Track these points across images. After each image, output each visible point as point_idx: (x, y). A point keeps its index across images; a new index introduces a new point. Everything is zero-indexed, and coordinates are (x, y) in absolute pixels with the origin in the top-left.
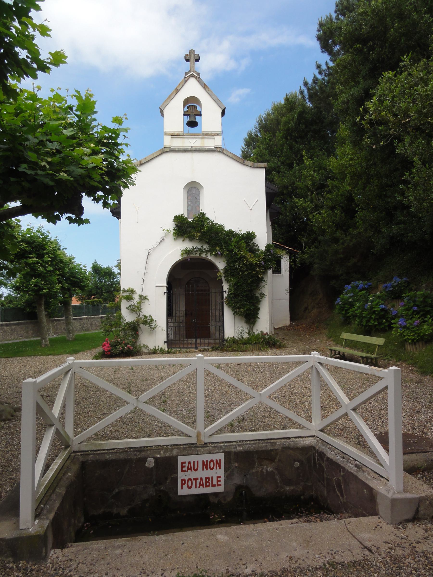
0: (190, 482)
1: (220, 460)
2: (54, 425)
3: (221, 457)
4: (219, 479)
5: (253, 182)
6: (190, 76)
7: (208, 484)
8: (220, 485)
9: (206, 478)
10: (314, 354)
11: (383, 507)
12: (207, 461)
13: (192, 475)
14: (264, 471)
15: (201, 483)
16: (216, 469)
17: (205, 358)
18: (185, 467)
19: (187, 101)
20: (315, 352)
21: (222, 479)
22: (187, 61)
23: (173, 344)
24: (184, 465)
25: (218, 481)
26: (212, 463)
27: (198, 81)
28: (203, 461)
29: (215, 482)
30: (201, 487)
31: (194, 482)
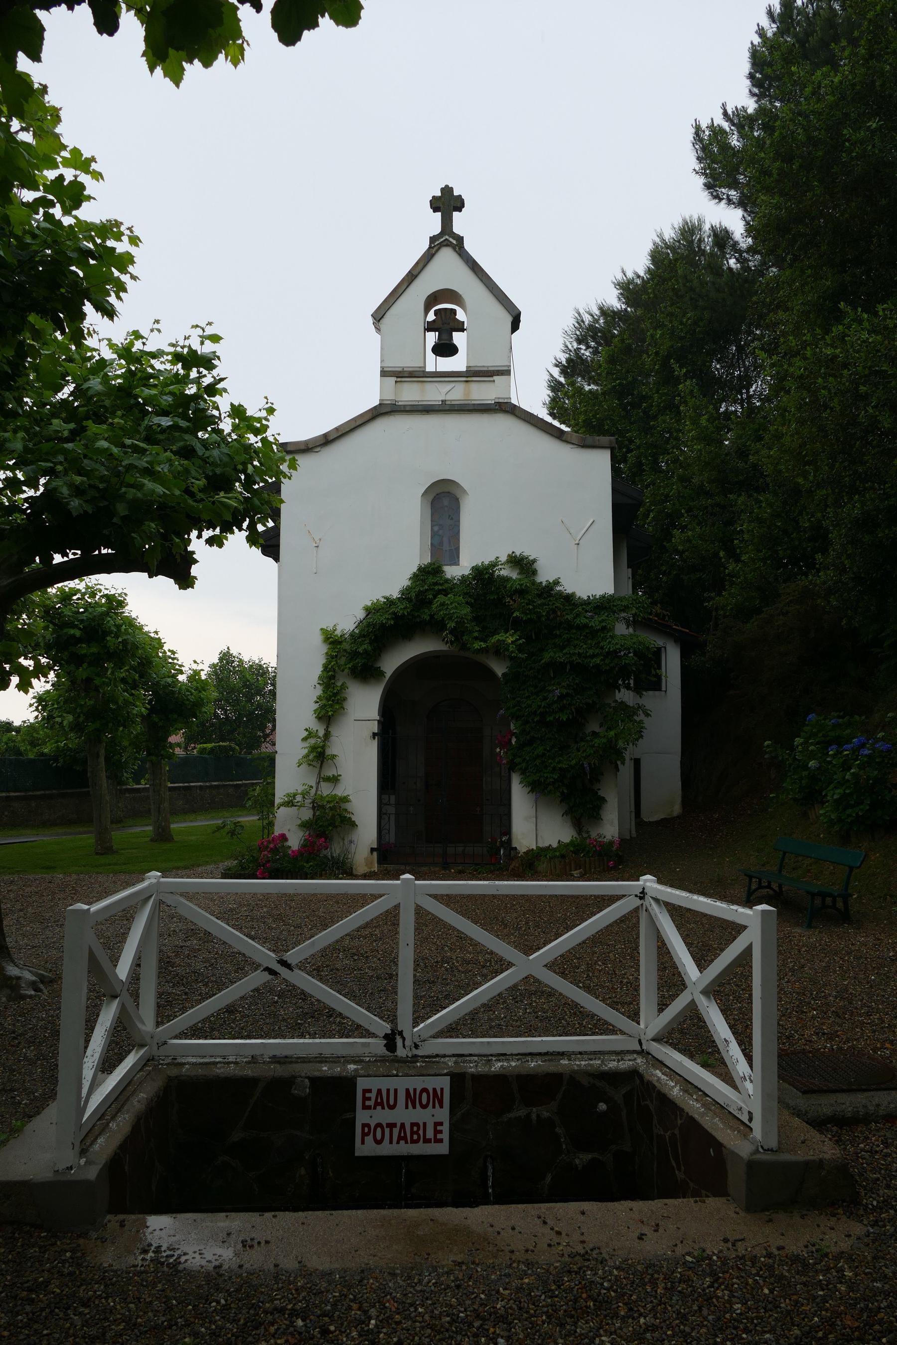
0: (379, 1130)
1: (442, 1089)
2: (117, 997)
3: (444, 1083)
4: (439, 1128)
5: (590, 474)
6: (441, 245)
7: (415, 1137)
8: (441, 1141)
9: (413, 1125)
10: (646, 881)
11: (736, 1178)
12: (415, 1090)
13: (382, 1116)
14: (534, 1116)
15: (402, 1135)
16: (434, 1107)
17: (417, 882)
18: (369, 1099)
19: (433, 300)
20: (648, 877)
21: (446, 1128)
22: (434, 211)
23: (390, 858)
24: (368, 1095)
25: (436, 1132)
26: (424, 1095)
27: (460, 255)
28: (407, 1090)
29: (430, 1134)
30: (402, 1142)
31: (387, 1131)
